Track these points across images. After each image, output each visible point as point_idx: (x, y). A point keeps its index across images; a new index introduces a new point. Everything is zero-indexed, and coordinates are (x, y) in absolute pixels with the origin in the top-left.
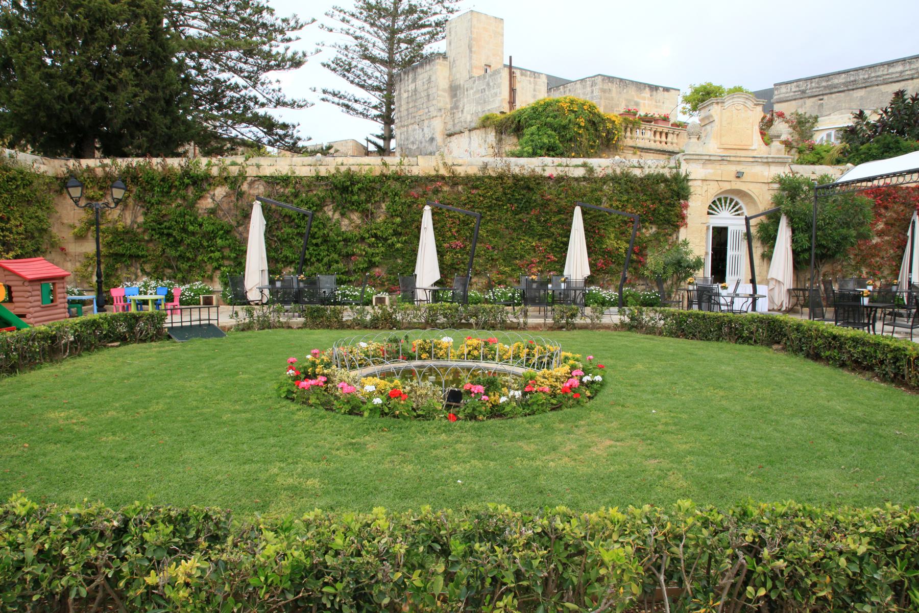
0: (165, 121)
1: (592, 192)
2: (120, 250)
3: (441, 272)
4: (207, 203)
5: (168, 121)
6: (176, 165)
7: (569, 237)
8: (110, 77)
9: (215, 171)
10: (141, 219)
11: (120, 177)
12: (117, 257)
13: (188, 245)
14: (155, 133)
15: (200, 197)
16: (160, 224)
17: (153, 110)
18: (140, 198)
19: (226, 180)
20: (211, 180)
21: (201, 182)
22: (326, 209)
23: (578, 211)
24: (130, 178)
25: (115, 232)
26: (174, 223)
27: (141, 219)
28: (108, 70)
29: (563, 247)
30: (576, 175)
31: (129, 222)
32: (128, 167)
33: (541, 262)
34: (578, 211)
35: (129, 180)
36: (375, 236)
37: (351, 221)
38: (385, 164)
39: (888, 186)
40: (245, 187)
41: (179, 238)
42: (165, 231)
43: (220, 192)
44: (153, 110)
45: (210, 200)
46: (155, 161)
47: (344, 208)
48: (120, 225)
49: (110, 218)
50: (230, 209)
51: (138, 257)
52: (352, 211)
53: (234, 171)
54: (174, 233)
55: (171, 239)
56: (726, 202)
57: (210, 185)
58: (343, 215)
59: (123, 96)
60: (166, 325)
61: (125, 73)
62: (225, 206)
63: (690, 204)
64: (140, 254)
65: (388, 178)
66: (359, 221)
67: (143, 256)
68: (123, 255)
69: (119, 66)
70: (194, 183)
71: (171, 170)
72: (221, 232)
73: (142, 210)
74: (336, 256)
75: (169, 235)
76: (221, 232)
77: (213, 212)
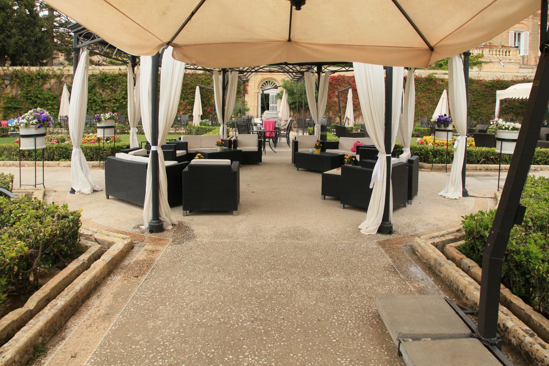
0: (35, 50)
1: (205, 80)
2: (10, 105)
3: (203, 112)
4: (48, 86)
5: (36, 49)
6: (35, 70)
7: (194, 99)
8: (8, 32)
9: (51, 73)
10: (19, 92)
11: (10, 74)
12: (8, 108)
13: (39, 103)
14: (30, 54)
15: (44, 84)
16: (27, 94)
17: (29, 45)
18: (19, 84)
19: (55, 76)
20: (49, 77)
21: (45, 77)
22: (96, 88)
23: (198, 88)
24: (15, 76)
25: (8, 98)
26: (33, 94)
27: (19, 92)
28: (7, 29)
29: (192, 104)
30: (199, 73)
31: (14, 93)
32: (14, 71)
33: (184, 109)
34: (198, 88)
35: (14, 76)
36: (115, 99)
37: (107, 93)
38: (120, 69)
39: (340, 76)
40: (63, 79)
41: (35, 100)
42: (29, 97)
43: (53, 81)
44: (29, 45)
45: (49, 85)
46: (26, 68)
47: (104, 88)
48: (10, 96)
49: (6, 92)
50: (57, 88)
51: (18, 108)
52: (107, 89)
53: (58, 72)
54: (33, 98)
55: (31, 101)
56: (271, 84)
57: (49, 78)
58: (103, 90)
59: (12, 41)
60: (508, 166)
61: (14, 31)
62: (55, 87)
63: (249, 84)
64: (18, 107)
65: (120, 75)
66: (110, 93)
67: (19, 108)
68: (11, 108)
69: (12, 28)
70: (42, 77)
71: (32, 73)
72: (52, 98)
73: (20, 89)
74: (98, 108)
75: (31, 99)
76: (52, 98)
77: (50, 89)
